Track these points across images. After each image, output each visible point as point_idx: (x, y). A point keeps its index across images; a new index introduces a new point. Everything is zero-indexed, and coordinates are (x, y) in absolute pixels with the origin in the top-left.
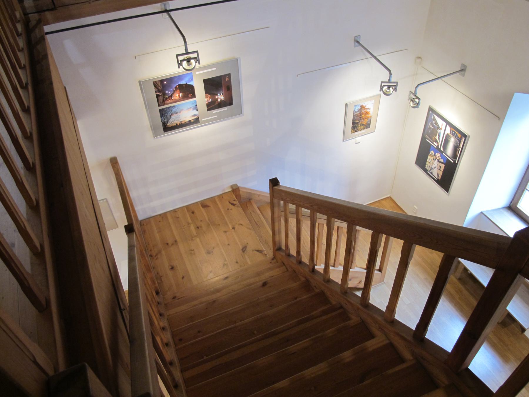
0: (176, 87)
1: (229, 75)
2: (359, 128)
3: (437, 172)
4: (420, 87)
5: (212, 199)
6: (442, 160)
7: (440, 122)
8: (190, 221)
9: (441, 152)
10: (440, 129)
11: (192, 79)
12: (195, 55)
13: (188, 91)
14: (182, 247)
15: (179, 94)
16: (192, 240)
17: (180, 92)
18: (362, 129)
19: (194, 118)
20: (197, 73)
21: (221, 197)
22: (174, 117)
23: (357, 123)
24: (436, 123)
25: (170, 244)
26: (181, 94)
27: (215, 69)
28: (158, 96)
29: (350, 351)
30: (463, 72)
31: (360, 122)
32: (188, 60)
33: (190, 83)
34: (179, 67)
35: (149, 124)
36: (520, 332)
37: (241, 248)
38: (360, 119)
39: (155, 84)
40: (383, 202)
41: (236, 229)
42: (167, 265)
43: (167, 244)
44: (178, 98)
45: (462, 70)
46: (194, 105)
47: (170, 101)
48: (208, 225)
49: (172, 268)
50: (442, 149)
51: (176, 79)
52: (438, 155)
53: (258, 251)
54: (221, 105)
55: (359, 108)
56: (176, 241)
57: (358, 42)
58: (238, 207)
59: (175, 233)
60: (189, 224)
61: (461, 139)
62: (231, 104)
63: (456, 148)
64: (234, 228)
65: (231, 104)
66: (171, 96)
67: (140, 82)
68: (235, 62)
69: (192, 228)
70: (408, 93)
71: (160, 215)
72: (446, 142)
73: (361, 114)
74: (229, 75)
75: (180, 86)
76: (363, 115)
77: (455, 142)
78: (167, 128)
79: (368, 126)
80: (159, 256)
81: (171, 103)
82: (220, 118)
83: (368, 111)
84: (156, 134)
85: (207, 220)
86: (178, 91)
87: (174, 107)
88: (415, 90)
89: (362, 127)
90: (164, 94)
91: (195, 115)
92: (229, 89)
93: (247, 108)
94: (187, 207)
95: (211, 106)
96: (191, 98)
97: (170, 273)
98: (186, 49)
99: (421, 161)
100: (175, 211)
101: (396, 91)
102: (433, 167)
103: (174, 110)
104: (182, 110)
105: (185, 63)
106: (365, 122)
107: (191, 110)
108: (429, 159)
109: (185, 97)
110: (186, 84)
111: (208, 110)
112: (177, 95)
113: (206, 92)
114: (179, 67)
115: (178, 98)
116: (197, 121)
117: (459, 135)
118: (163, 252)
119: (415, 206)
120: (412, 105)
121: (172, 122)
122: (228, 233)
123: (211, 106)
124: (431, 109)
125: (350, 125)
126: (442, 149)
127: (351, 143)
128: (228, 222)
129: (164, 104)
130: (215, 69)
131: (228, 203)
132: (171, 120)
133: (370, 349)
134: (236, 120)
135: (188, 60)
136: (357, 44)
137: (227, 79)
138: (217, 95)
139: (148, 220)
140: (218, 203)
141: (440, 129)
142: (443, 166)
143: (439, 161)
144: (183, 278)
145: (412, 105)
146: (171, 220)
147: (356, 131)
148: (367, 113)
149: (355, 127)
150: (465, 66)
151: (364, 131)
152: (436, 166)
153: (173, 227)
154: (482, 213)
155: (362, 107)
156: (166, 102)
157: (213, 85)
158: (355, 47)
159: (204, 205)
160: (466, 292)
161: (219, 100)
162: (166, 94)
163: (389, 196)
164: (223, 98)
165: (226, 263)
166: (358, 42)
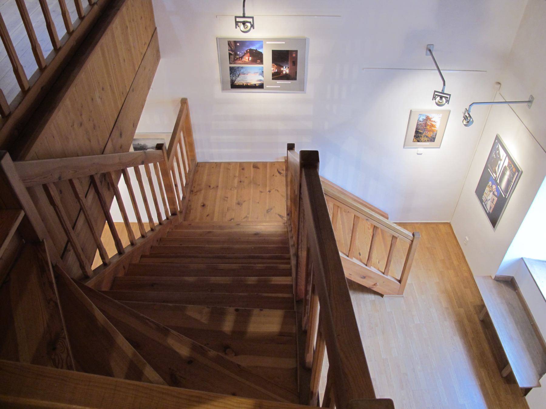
0: (247, 51)
1: (296, 51)
2: (422, 139)
3: (490, 206)
4: (474, 106)
5: (265, 164)
6: (496, 193)
7: (502, 153)
8: (237, 174)
9: (497, 185)
10: (501, 160)
11: (262, 47)
12: (250, 20)
13: (257, 57)
14: (220, 193)
15: (248, 57)
16: (231, 189)
17: (250, 56)
18: (425, 141)
19: (260, 83)
20: (267, 43)
21: (272, 164)
22: (241, 77)
23: (421, 133)
24: (499, 154)
25: (212, 187)
26: (250, 58)
27: (284, 43)
28: (230, 54)
29: (256, 278)
30: (530, 104)
31: (423, 133)
32: (441, 98)
33: (260, 50)
34: (236, 28)
35: (219, 77)
36: (522, 395)
37: (267, 208)
38: (425, 129)
39: (229, 43)
40: (441, 226)
41: (271, 192)
42: (201, 201)
43: (210, 186)
44: (247, 61)
45: (529, 101)
46: (261, 71)
47: (240, 62)
48: (250, 183)
49: (204, 206)
50: (498, 181)
51: (247, 44)
52: (494, 187)
53: (280, 216)
54: (287, 77)
55: (425, 118)
56: (217, 186)
57: (430, 50)
58: (283, 176)
59: (220, 180)
60: (235, 176)
61: (515, 173)
62: (295, 79)
63: (509, 182)
64: (270, 191)
65: (295, 79)
66: (242, 58)
67: (217, 38)
68: (303, 41)
69: (236, 181)
70: (464, 110)
71: (216, 163)
72: (503, 174)
73: (426, 125)
74: (296, 51)
75: (251, 50)
76: (428, 127)
77: (510, 176)
78: (234, 86)
79: (433, 139)
80: (198, 193)
81: (240, 64)
82: (284, 89)
83: (433, 123)
84: (224, 89)
85: (252, 178)
86: (248, 54)
87: (242, 67)
88: (469, 108)
89: (426, 139)
90: (236, 54)
91: (260, 80)
92: (295, 63)
93: (310, 87)
94: (241, 164)
95: (277, 76)
96: (259, 64)
97: (199, 209)
98: (244, 14)
99: (480, 192)
100: (229, 163)
101: (254, 28)
102: (488, 198)
103: (242, 70)
104: (249, 73)
105: (242, 26)
106: (430, 134)
107: (258, 74)
108: (487, 189)
109: (254, 62)
110: (256, 50)
111: (273, 79)
112: (247, 58)
113: (273, 63)
114: (236, 28)
115: (247, 61)
116: (261, 86)
117: (514, 169)
118: (203, 191)
119: (467, 237)
120: (465, 123)
121: (239, 81)
122: (262, 194)
123: (277, 76)
124: (497, 138)
125: (413, 133)
126: (498, 181)
127: (413, 151)
128: (268, 185)
129: (235, 63)
130: (284, 43)
131: (276, 170)
132: (238, 79)
133: (273, 283)
134: (298, 96)
135: (441, 98)
136: (429, 52)
137: (294, 55)
138: (283, 67)
139: (204, 164)
140: (268, 168)
141: (501, 160)
142: (496, 199)
143: (494, 194)
144: (208, 215)
145: (465, 123)
146: (222, 170)
147: (418, 141)
148: (432, 126)
149: (418, 136)
150: (532, 97)
151: (428, 143)
152: (490, 197)
153: (221, 175)
154: (522, 258)
155: (428, 118)
156: (236, 62)
157: (281, 57)
158: (426, 55)
159: (255, 166)
160: (483, 336)
161: (284, 72)
162: (238, 55)
163: (449, 222)
164: (288, 71)
165: (248, 216)
166: (430, 50)
